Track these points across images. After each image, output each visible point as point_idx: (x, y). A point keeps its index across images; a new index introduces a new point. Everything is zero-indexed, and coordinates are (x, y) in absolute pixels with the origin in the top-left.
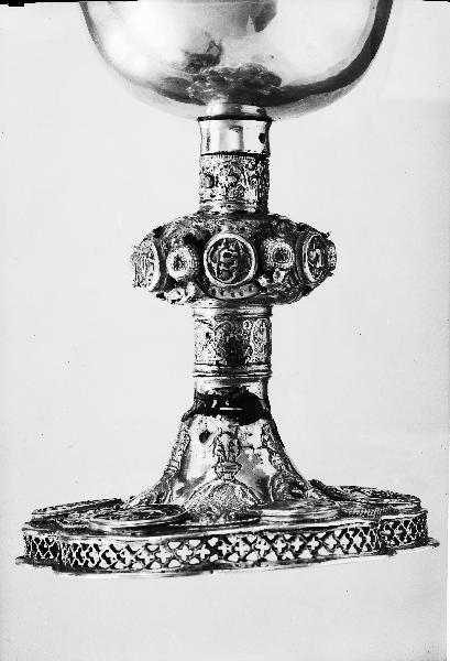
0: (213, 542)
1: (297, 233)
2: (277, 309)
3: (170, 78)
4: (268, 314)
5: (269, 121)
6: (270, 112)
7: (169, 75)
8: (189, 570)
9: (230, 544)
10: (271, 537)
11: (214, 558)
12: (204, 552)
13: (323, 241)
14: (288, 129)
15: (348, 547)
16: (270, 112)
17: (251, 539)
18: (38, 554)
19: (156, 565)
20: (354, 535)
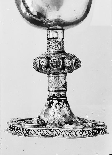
0: (52, 130)
1: (72, 57)
2: (67, 75)
3: (39, 5)
4: (66, 76)
5: (64, 30)
6: (64, 28)
7: (39, 4)
8: (47, 136)
9: (56, 131)
10: (57, 131)
11: (52, 134)
12: (50, 132)
13: (77, 60)
14: (69, 31)
15: (85, 134)
16: (64, 28)
17: (57, 131)
18: (12, 128)
19: (61, 135)
20: (25, 133)
